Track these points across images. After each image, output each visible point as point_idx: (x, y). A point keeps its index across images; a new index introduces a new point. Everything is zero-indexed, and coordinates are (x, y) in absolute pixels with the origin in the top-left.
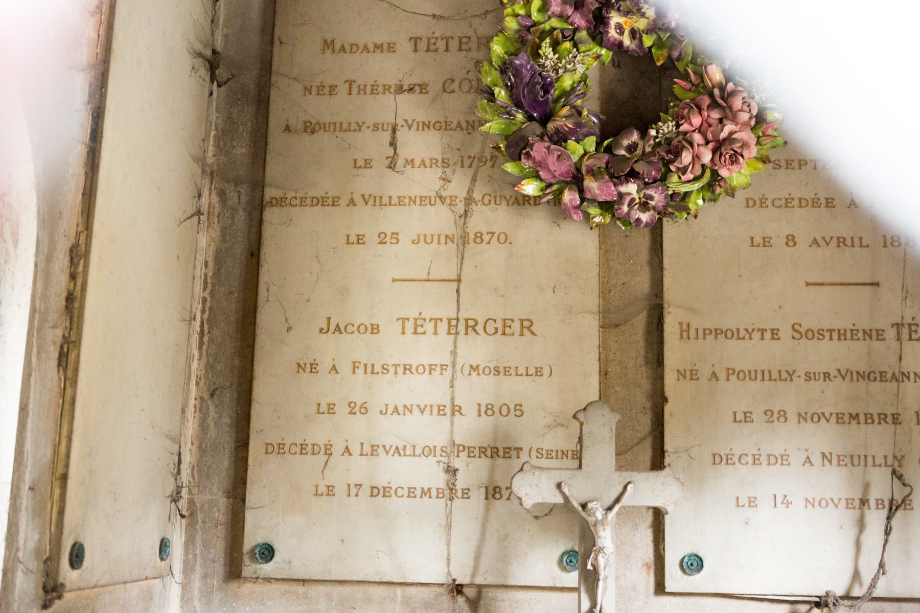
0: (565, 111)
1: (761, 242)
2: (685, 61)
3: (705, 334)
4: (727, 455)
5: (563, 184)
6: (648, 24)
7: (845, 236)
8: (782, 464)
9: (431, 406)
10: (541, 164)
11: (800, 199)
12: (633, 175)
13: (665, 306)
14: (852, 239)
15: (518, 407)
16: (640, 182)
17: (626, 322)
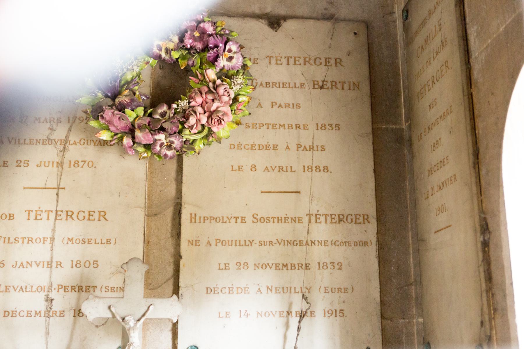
0: (126, 92)
1: (237, 169)
2: (196, 67)
3: (204, 220)
4: (215, 288)
5: (124, 134)
6: (175, 46)
7: (283, 166)
8: (245, 293)
9: (44, 262)
10: (110, 122)
11: (259, 145)
12: (162, 129)
13: (183, 204)
14: (287, 167)
15: (95, 262)
16: (167, 134)
17: (161, 213)
